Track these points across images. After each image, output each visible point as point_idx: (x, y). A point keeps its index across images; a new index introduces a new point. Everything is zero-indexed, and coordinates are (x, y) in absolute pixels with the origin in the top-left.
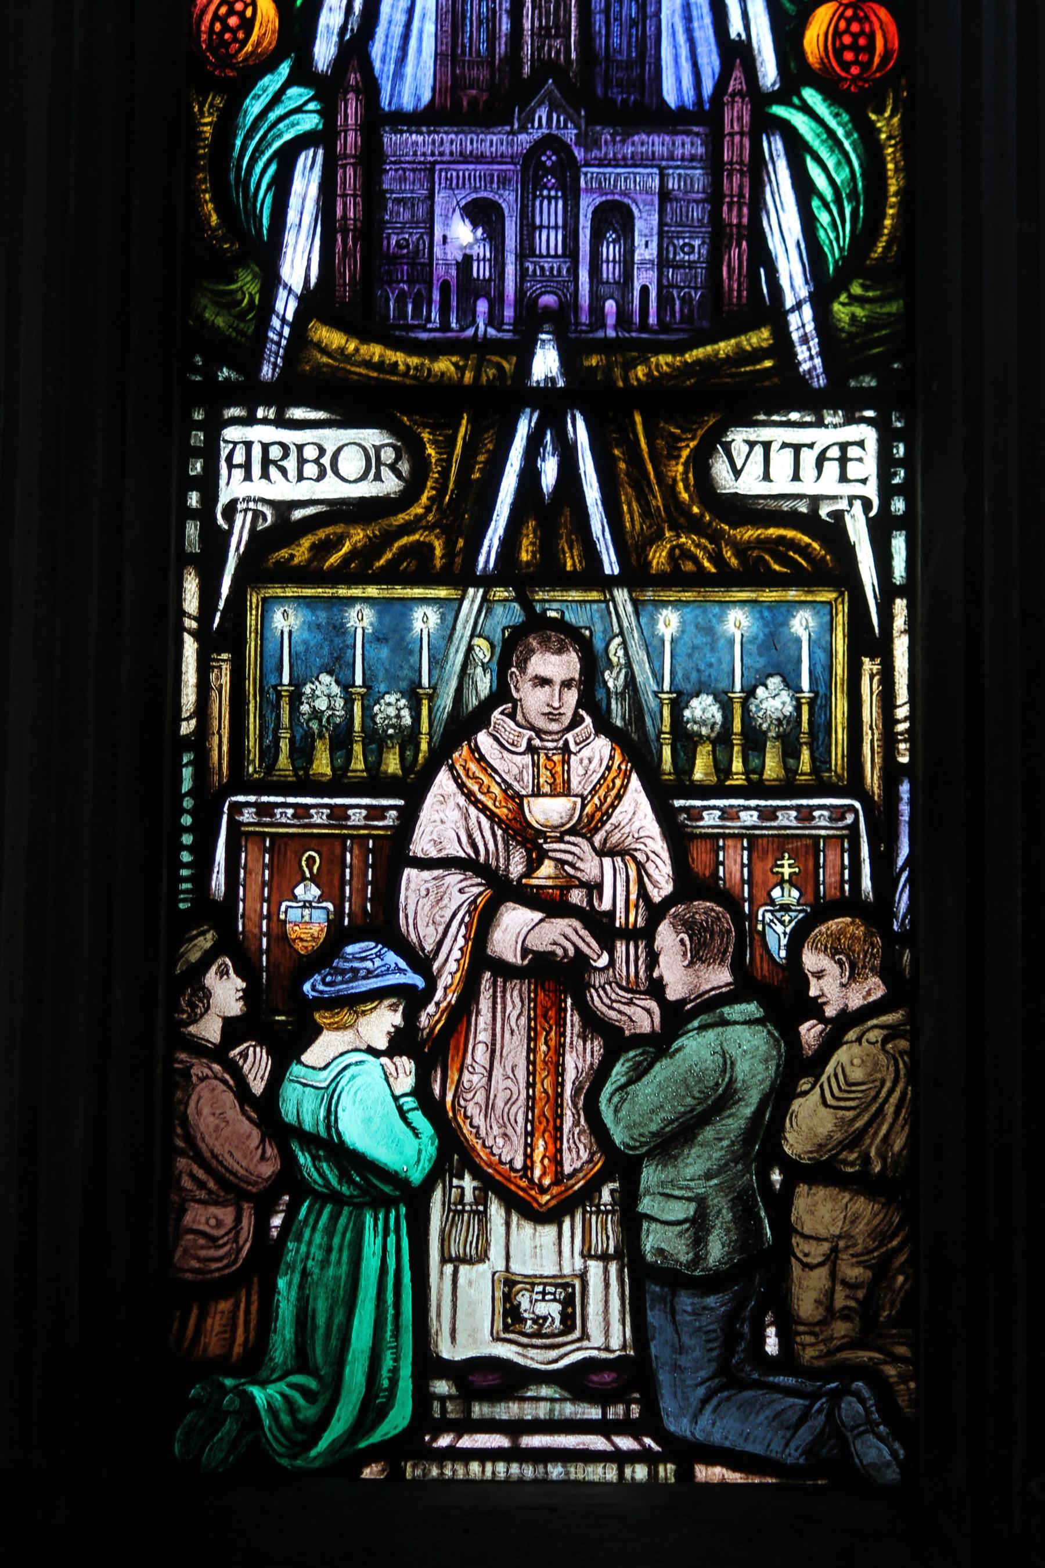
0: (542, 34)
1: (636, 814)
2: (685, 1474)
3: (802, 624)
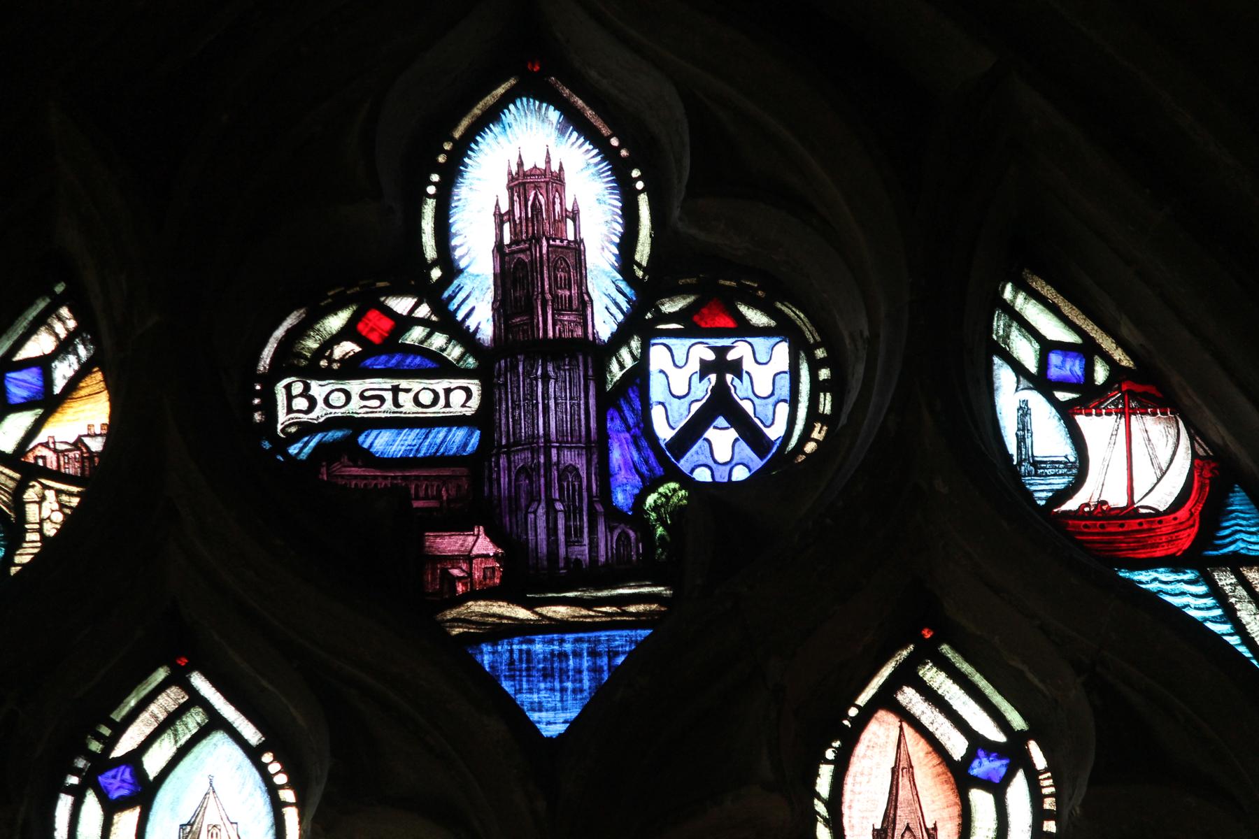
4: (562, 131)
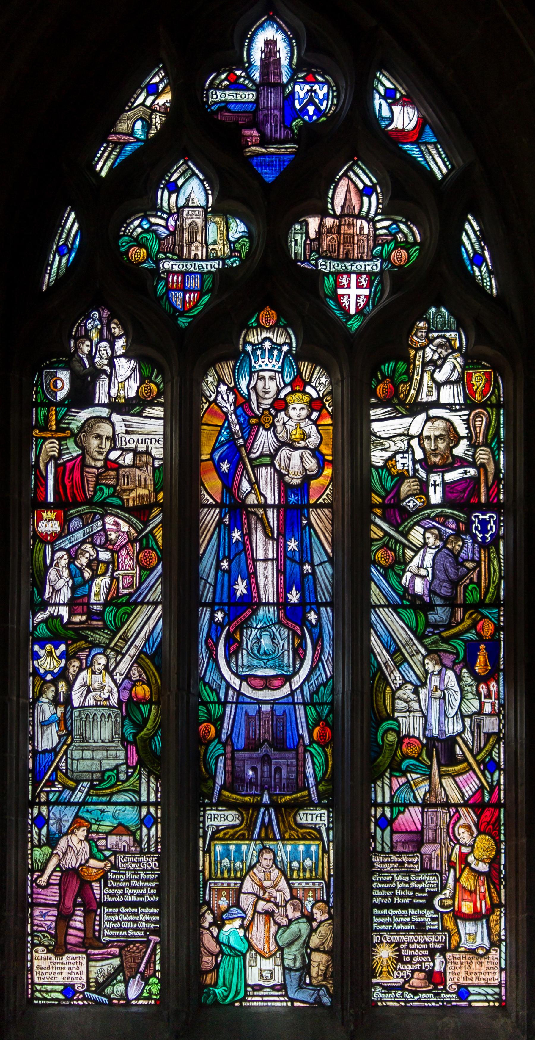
0: (264, 733)
1: (283, 884)
2: (292, 1004)
3: (313, 848)
4: (277, 31)
